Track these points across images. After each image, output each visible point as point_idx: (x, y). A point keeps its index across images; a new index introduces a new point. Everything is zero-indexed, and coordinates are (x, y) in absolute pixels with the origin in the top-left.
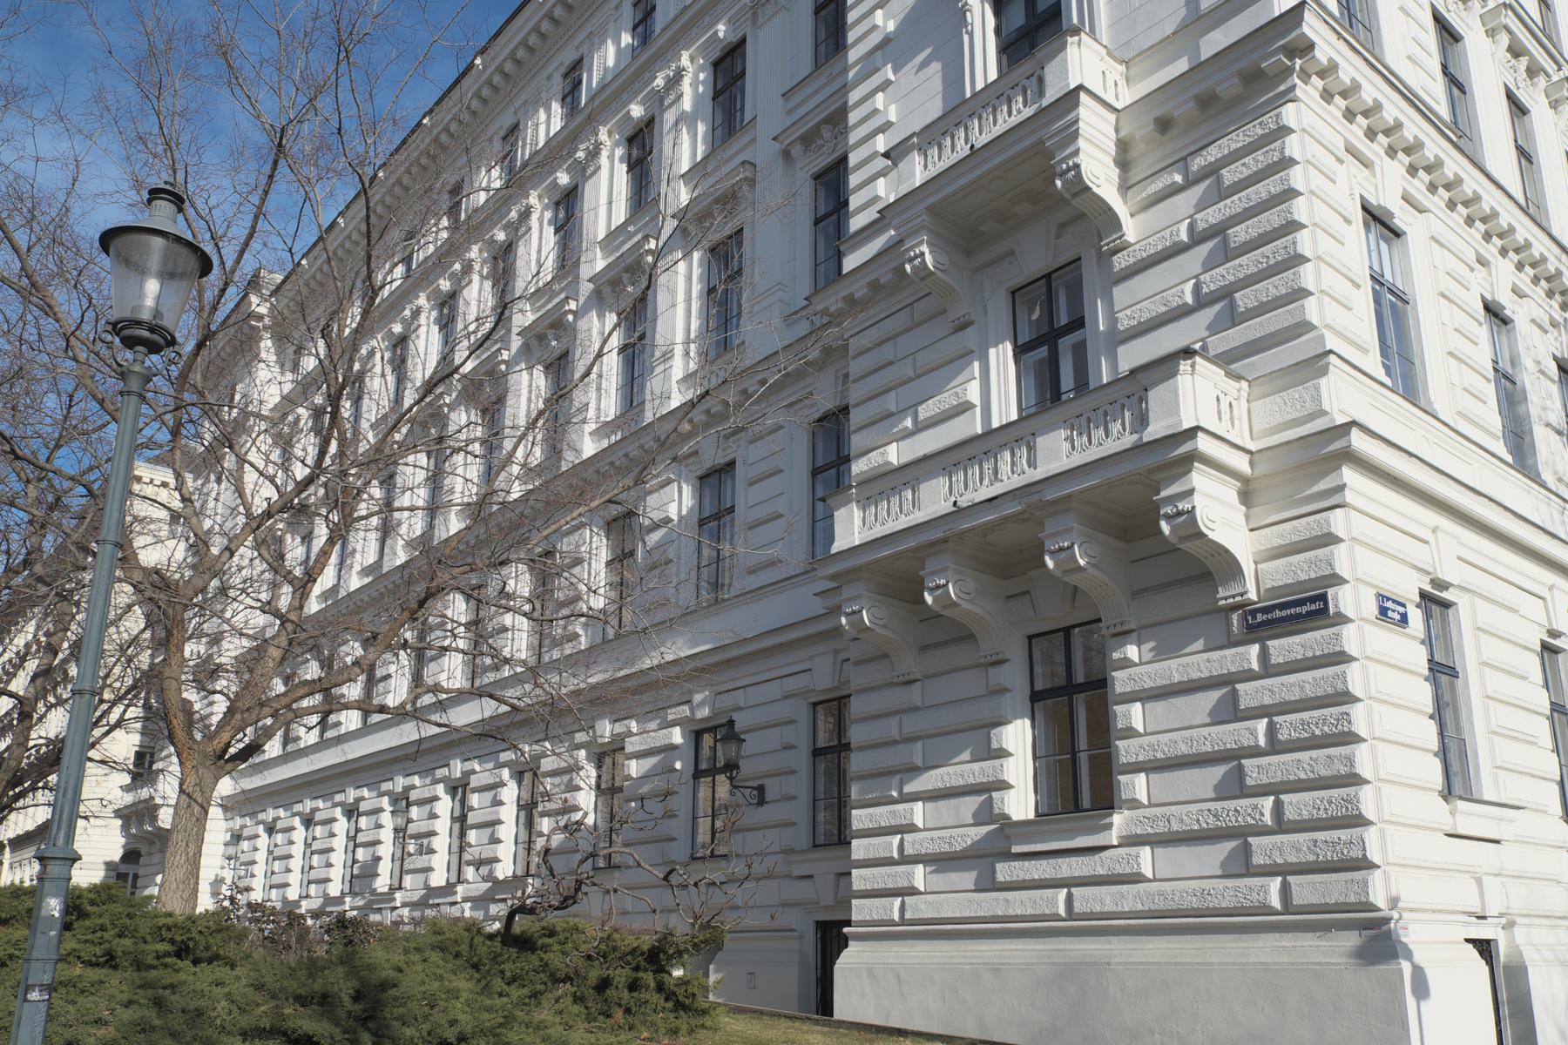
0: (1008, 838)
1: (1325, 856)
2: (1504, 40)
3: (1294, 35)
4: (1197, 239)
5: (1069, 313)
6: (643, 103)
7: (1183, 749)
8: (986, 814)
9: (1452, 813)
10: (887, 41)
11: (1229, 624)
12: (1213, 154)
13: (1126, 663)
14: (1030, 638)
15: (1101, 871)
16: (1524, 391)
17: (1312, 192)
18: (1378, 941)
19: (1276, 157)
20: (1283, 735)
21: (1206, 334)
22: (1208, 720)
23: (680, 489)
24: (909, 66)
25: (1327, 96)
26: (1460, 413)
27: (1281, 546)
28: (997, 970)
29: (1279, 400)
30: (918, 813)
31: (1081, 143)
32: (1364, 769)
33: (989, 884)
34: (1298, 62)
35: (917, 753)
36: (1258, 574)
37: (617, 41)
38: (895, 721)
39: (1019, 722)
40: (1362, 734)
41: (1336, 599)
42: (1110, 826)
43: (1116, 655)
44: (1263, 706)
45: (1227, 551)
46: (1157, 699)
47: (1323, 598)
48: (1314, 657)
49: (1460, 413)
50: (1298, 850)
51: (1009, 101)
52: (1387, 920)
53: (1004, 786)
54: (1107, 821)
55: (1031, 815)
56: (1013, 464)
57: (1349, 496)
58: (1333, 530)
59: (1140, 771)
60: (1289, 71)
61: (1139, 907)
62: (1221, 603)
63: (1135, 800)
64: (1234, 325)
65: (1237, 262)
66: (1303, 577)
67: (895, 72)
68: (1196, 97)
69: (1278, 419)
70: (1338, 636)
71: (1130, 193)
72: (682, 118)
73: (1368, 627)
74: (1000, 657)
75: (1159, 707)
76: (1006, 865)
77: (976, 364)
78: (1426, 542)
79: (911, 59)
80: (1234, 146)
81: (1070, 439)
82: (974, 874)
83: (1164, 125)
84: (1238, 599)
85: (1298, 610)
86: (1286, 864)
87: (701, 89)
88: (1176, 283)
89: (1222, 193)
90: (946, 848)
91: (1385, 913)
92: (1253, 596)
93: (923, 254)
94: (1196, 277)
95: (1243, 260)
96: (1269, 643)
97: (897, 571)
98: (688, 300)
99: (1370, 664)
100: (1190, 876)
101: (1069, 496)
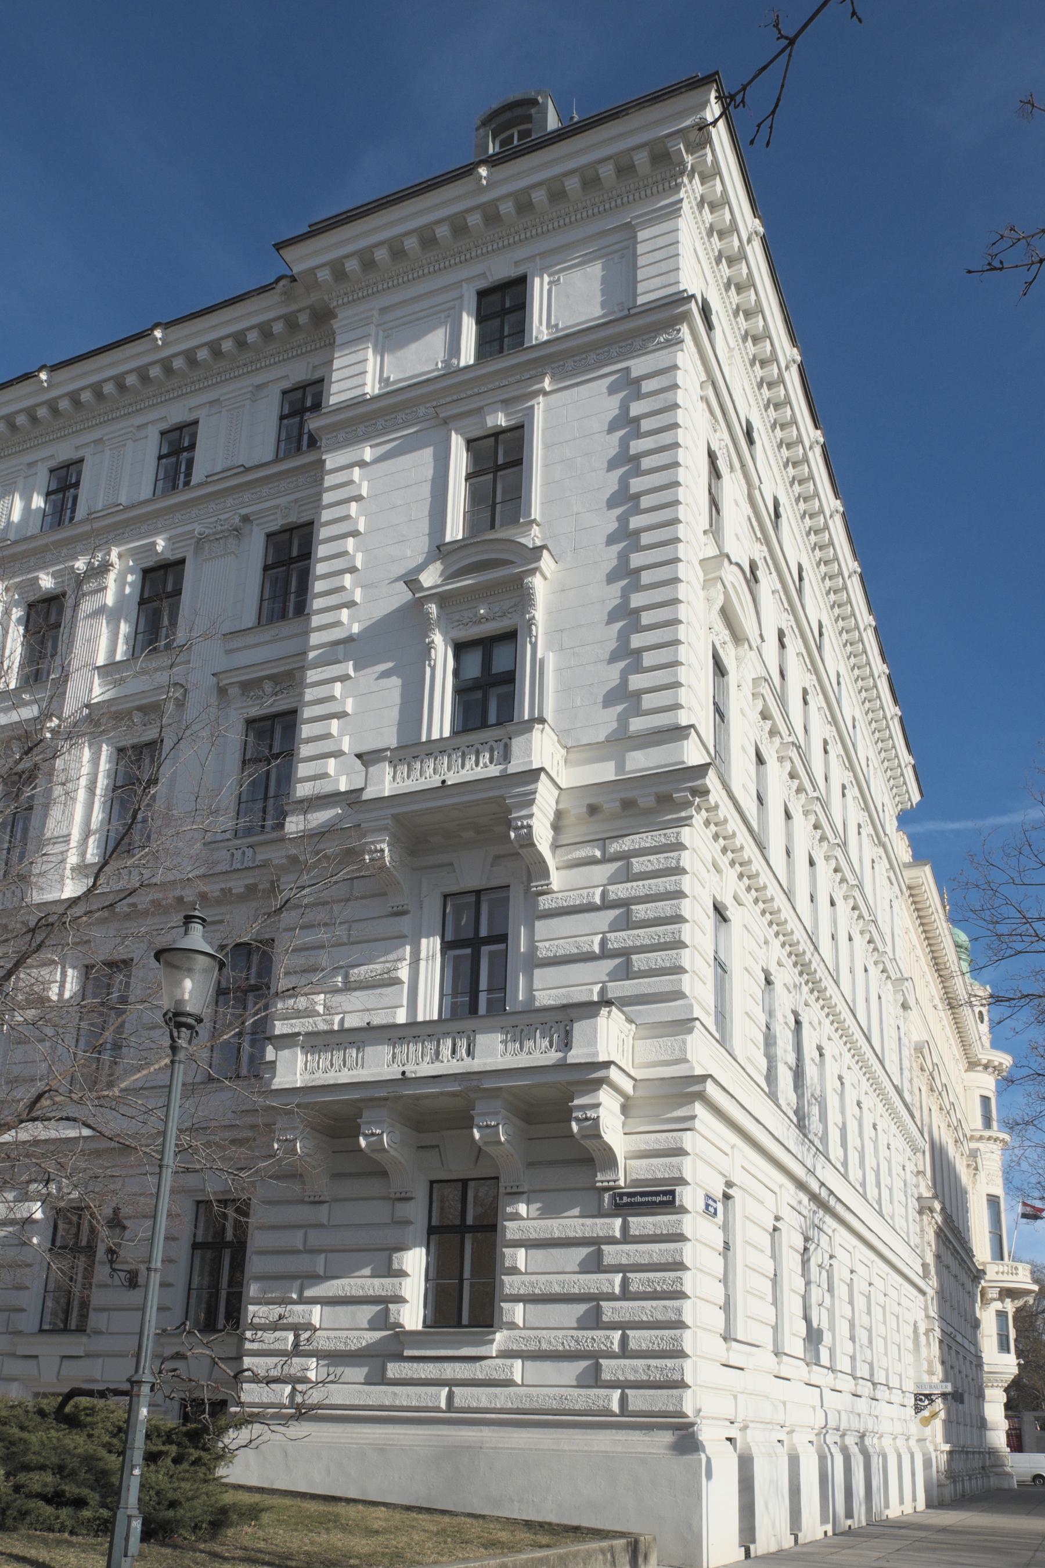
0: (401, 1343)
1: (655, 1377)
2: (788, 766)
3: (699, 782)
4: (607, 905)
5: (490, 926)
6: (54, 575)
7: (557, 1289)
8: (383, 1321)
9: (728, 1350)
10: (350, 639)
11: (601, 1201)
12: (626, 844)
13: (516, 1217)
14: (432, 1182)
15: (480, 1376)
16: (775, 1037)
17: (694, 897)
18: (686, 1440)
19: (674, 864)
20: (633, 1288)
21: (607, 979)
22: (577, 1269)
23: (64, 974)
24: (369, 670)
25: (707, 823)
26: (748, 1059)
27: (646, 1150)
28: (382, 1450)
29: (656, 1044)
30: (316, 1314)
31: (535, 809)
32: (687, 1318)
33: (378, 1378)
34: (697, 799)
35: (319, 1264)
36: (629, 1170)
37: (28, 501)
38: (300, 1234)
39: (418, 1250)
40: (689, 1293)
41: (681, 1195)
42: (492, 1341)
43: (509, 1210)
44: (621, 1265)
45: (611, 1149)
46: (536, 1247)
47: (672, 1193)
48: (662, 1234)
49: (748, 1059)
50: (636, 1372)
51: (478, 753)
52: (692, 1424)
53: (400, 1300)
54: (490, 1337)
55: (420, 1327)
56: (454, 1052)
57: (697, 1124)
58: (684, 1146)
59: (519, 1301)
60: (690, 804)
61: (509, 1405)
62: (599, 1184)
63: (514, 1323)
64: (628, 979)
65: (636, 932)
66: (659, 1176)
67: (356, 670)
68: (622, 799)
69: (653, 1057)
70: (680, 1222)
71: (559, 851)
72: (102, 610)
73: (699, 1219)
74: (409, 1195)
75: (539, 1254)
76: (397, 1365)
77: (408, 948)
78: (727, 1155)
79: (374, 665)
80: (643, 845)
81: (505, 1042)
82: (365, 1370)
83: (593, 810)
84: (612, 1184)
85: (654, 1199)
86: (626, 1380)
87: (128, 590)
88: (589, 932)
89: (628, 876)
90: (341, 1347)
91: (691, 1420)
92: (622, 1183)
93: (382, 851)
94: (603, 933)
95: (640, 932)
96: (630, 1219)
97: (337, 1118)
98: (91, 790)
99: (697, 1244)
100: (554, 1384)
101: (501, 1088)
